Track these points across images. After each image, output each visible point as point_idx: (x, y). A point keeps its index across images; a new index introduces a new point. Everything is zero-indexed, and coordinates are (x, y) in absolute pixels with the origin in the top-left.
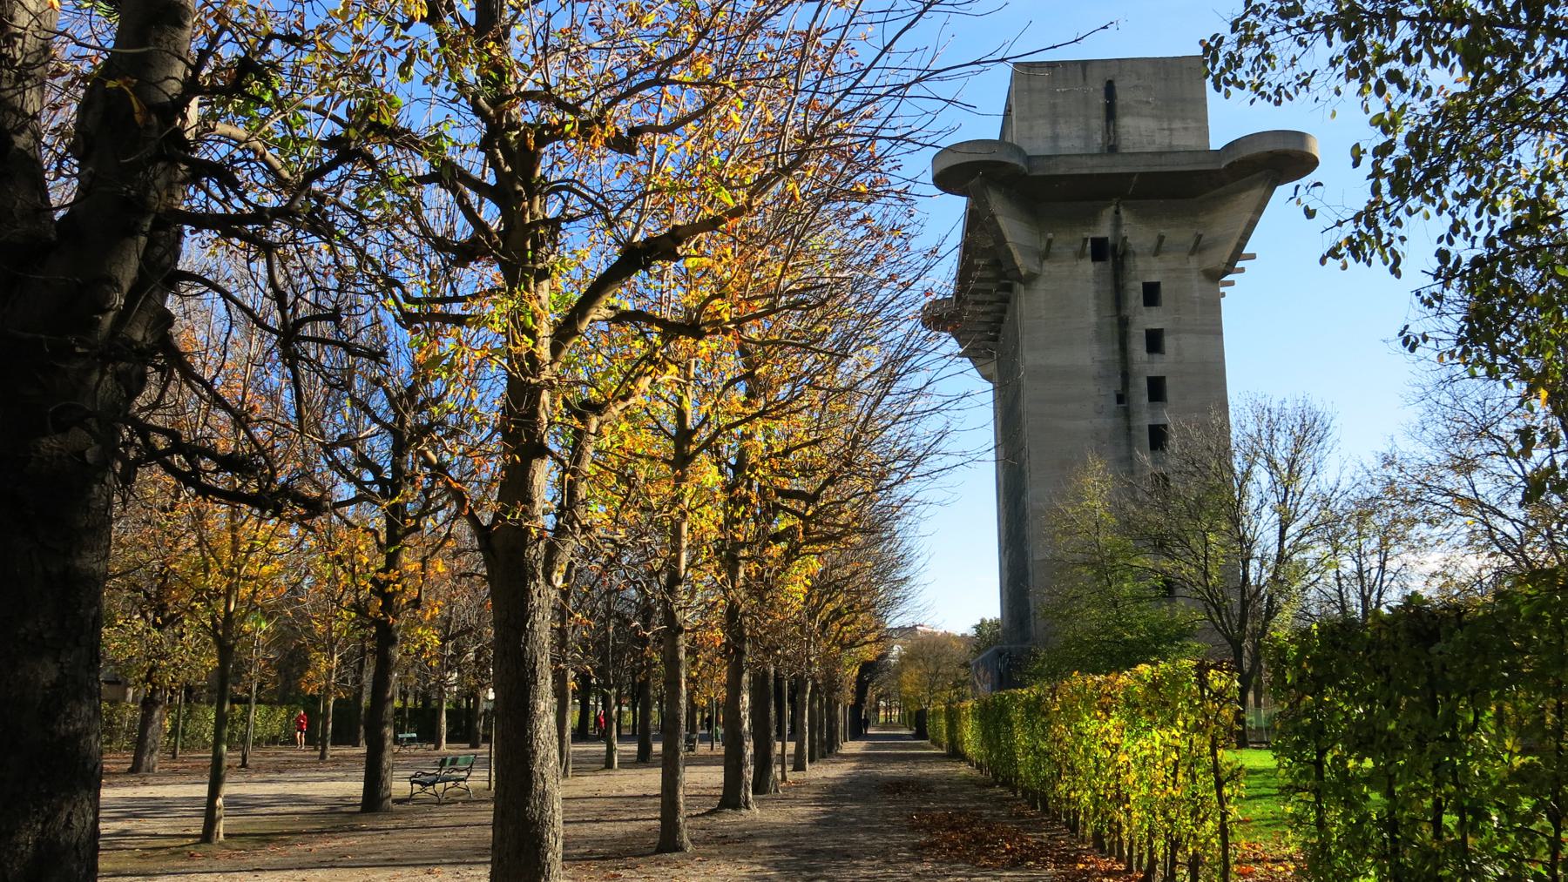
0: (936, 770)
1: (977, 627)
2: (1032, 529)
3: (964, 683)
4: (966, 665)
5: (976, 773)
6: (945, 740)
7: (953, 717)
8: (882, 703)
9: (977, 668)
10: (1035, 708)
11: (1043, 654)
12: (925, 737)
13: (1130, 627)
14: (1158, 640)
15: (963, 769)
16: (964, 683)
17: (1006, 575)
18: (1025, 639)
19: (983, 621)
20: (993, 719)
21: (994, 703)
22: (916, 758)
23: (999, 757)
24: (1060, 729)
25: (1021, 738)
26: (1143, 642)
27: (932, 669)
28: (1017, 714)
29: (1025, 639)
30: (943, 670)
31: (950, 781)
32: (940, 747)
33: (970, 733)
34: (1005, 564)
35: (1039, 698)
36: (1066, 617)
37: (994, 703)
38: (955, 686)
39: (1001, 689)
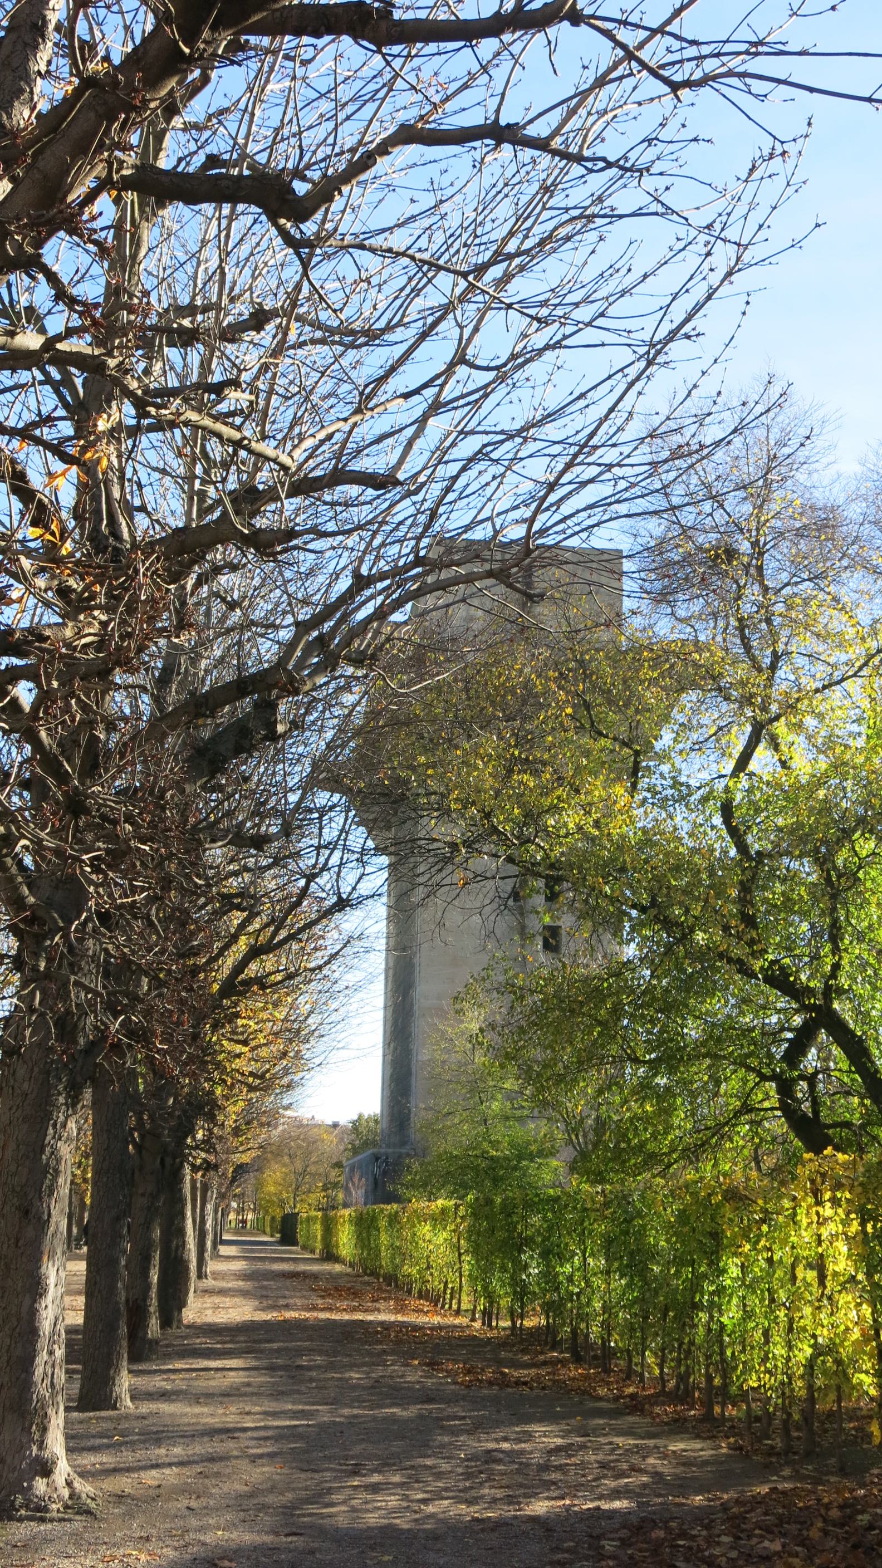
0: (315, 1268)
1: (354, 1122)
2: (421, 1025)
3: (335, 1185)
4: (338, 1165)
5: (349, 1270)
6: (319, 1246)
7: (329, 1228)
8: (234, 1205)
9: (352, 1169)
10: (394, 1219)
11: (416, 1166)
12: (295, 1243)
13: (495, 1144)
14: (520, 1157)
15: (338, 1268)
16: (335, 1185)
17: (387, 1093)
18: (403, 1143)
19: (360, 1116)
20: (365, 1226)
21: (368, 1213)
22: (294, 1260)
23: (369, 1254)
24: (406, 1233)
25: (384, 1238)
26: (506, 1158)
27: (299, 1165)
28: (383, 1223)
29: (403, 1143)
30: (312, 1169)
31: (330, 1273)
32: (313, 1252)
33: (345, 1240)
34: (388, 1073)
35: (397, 1212)
36: (440, 1131)
37: (368, 1213)
38: (325, 1188)
39: (374, 1203)
